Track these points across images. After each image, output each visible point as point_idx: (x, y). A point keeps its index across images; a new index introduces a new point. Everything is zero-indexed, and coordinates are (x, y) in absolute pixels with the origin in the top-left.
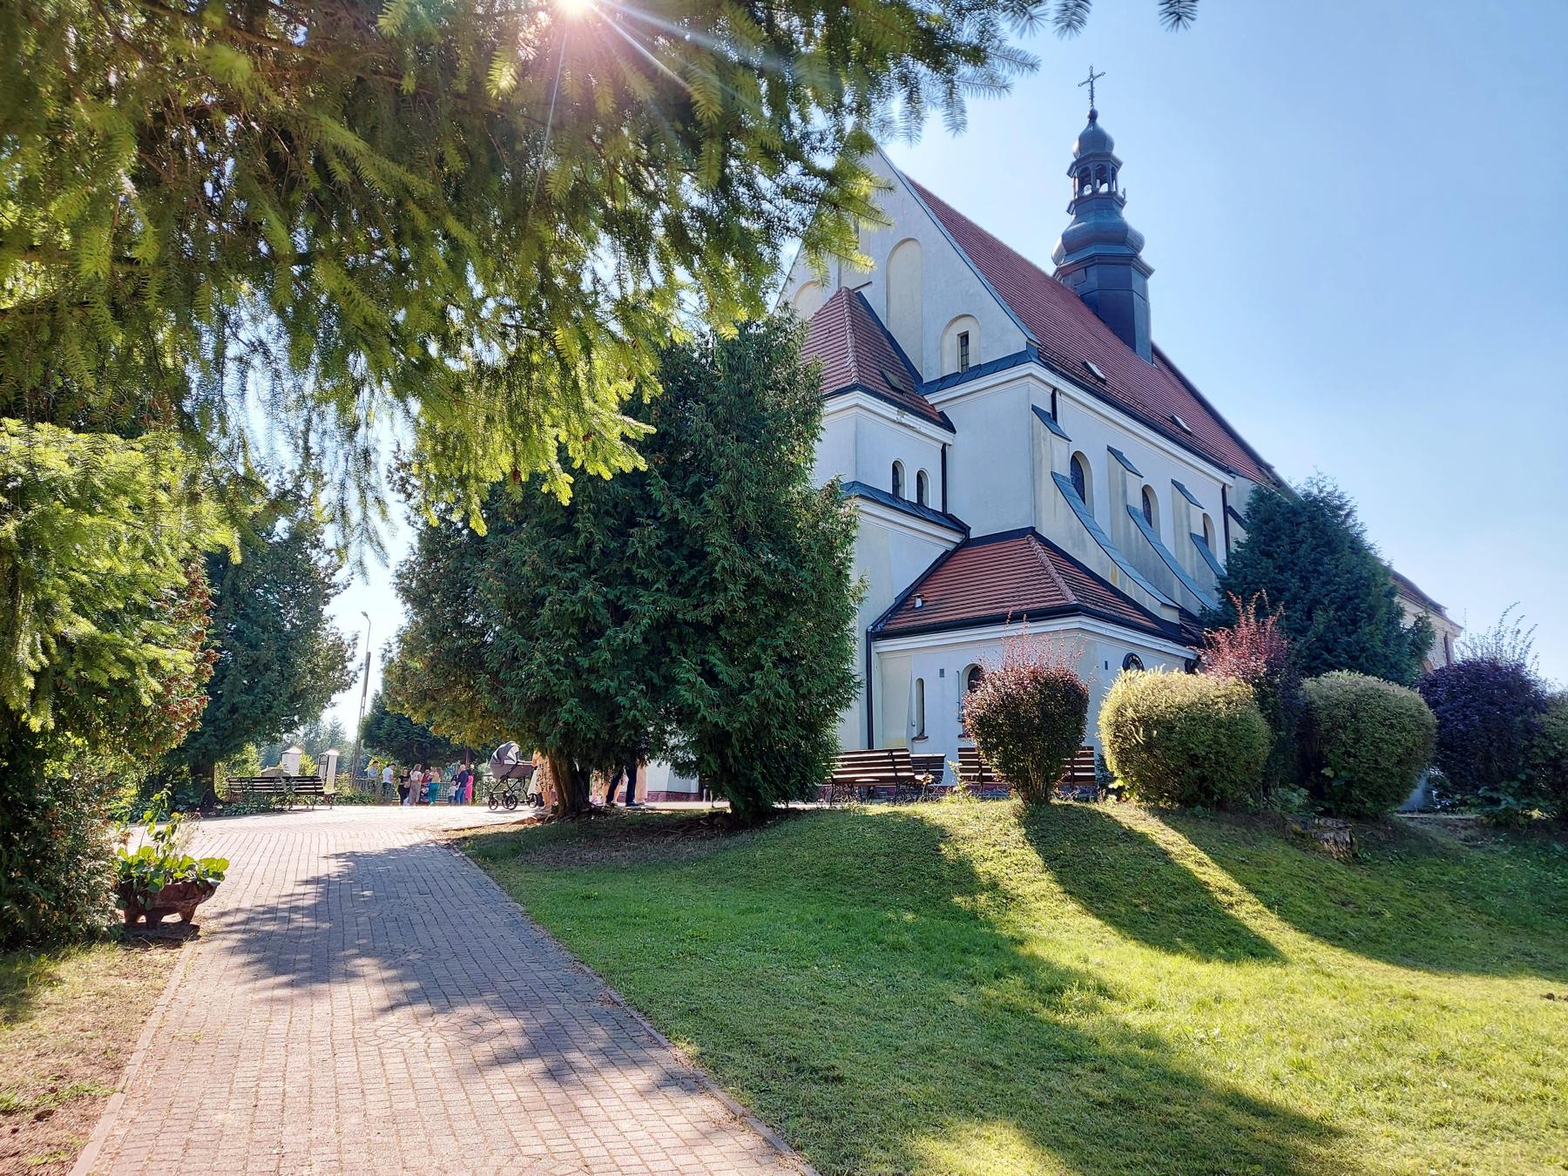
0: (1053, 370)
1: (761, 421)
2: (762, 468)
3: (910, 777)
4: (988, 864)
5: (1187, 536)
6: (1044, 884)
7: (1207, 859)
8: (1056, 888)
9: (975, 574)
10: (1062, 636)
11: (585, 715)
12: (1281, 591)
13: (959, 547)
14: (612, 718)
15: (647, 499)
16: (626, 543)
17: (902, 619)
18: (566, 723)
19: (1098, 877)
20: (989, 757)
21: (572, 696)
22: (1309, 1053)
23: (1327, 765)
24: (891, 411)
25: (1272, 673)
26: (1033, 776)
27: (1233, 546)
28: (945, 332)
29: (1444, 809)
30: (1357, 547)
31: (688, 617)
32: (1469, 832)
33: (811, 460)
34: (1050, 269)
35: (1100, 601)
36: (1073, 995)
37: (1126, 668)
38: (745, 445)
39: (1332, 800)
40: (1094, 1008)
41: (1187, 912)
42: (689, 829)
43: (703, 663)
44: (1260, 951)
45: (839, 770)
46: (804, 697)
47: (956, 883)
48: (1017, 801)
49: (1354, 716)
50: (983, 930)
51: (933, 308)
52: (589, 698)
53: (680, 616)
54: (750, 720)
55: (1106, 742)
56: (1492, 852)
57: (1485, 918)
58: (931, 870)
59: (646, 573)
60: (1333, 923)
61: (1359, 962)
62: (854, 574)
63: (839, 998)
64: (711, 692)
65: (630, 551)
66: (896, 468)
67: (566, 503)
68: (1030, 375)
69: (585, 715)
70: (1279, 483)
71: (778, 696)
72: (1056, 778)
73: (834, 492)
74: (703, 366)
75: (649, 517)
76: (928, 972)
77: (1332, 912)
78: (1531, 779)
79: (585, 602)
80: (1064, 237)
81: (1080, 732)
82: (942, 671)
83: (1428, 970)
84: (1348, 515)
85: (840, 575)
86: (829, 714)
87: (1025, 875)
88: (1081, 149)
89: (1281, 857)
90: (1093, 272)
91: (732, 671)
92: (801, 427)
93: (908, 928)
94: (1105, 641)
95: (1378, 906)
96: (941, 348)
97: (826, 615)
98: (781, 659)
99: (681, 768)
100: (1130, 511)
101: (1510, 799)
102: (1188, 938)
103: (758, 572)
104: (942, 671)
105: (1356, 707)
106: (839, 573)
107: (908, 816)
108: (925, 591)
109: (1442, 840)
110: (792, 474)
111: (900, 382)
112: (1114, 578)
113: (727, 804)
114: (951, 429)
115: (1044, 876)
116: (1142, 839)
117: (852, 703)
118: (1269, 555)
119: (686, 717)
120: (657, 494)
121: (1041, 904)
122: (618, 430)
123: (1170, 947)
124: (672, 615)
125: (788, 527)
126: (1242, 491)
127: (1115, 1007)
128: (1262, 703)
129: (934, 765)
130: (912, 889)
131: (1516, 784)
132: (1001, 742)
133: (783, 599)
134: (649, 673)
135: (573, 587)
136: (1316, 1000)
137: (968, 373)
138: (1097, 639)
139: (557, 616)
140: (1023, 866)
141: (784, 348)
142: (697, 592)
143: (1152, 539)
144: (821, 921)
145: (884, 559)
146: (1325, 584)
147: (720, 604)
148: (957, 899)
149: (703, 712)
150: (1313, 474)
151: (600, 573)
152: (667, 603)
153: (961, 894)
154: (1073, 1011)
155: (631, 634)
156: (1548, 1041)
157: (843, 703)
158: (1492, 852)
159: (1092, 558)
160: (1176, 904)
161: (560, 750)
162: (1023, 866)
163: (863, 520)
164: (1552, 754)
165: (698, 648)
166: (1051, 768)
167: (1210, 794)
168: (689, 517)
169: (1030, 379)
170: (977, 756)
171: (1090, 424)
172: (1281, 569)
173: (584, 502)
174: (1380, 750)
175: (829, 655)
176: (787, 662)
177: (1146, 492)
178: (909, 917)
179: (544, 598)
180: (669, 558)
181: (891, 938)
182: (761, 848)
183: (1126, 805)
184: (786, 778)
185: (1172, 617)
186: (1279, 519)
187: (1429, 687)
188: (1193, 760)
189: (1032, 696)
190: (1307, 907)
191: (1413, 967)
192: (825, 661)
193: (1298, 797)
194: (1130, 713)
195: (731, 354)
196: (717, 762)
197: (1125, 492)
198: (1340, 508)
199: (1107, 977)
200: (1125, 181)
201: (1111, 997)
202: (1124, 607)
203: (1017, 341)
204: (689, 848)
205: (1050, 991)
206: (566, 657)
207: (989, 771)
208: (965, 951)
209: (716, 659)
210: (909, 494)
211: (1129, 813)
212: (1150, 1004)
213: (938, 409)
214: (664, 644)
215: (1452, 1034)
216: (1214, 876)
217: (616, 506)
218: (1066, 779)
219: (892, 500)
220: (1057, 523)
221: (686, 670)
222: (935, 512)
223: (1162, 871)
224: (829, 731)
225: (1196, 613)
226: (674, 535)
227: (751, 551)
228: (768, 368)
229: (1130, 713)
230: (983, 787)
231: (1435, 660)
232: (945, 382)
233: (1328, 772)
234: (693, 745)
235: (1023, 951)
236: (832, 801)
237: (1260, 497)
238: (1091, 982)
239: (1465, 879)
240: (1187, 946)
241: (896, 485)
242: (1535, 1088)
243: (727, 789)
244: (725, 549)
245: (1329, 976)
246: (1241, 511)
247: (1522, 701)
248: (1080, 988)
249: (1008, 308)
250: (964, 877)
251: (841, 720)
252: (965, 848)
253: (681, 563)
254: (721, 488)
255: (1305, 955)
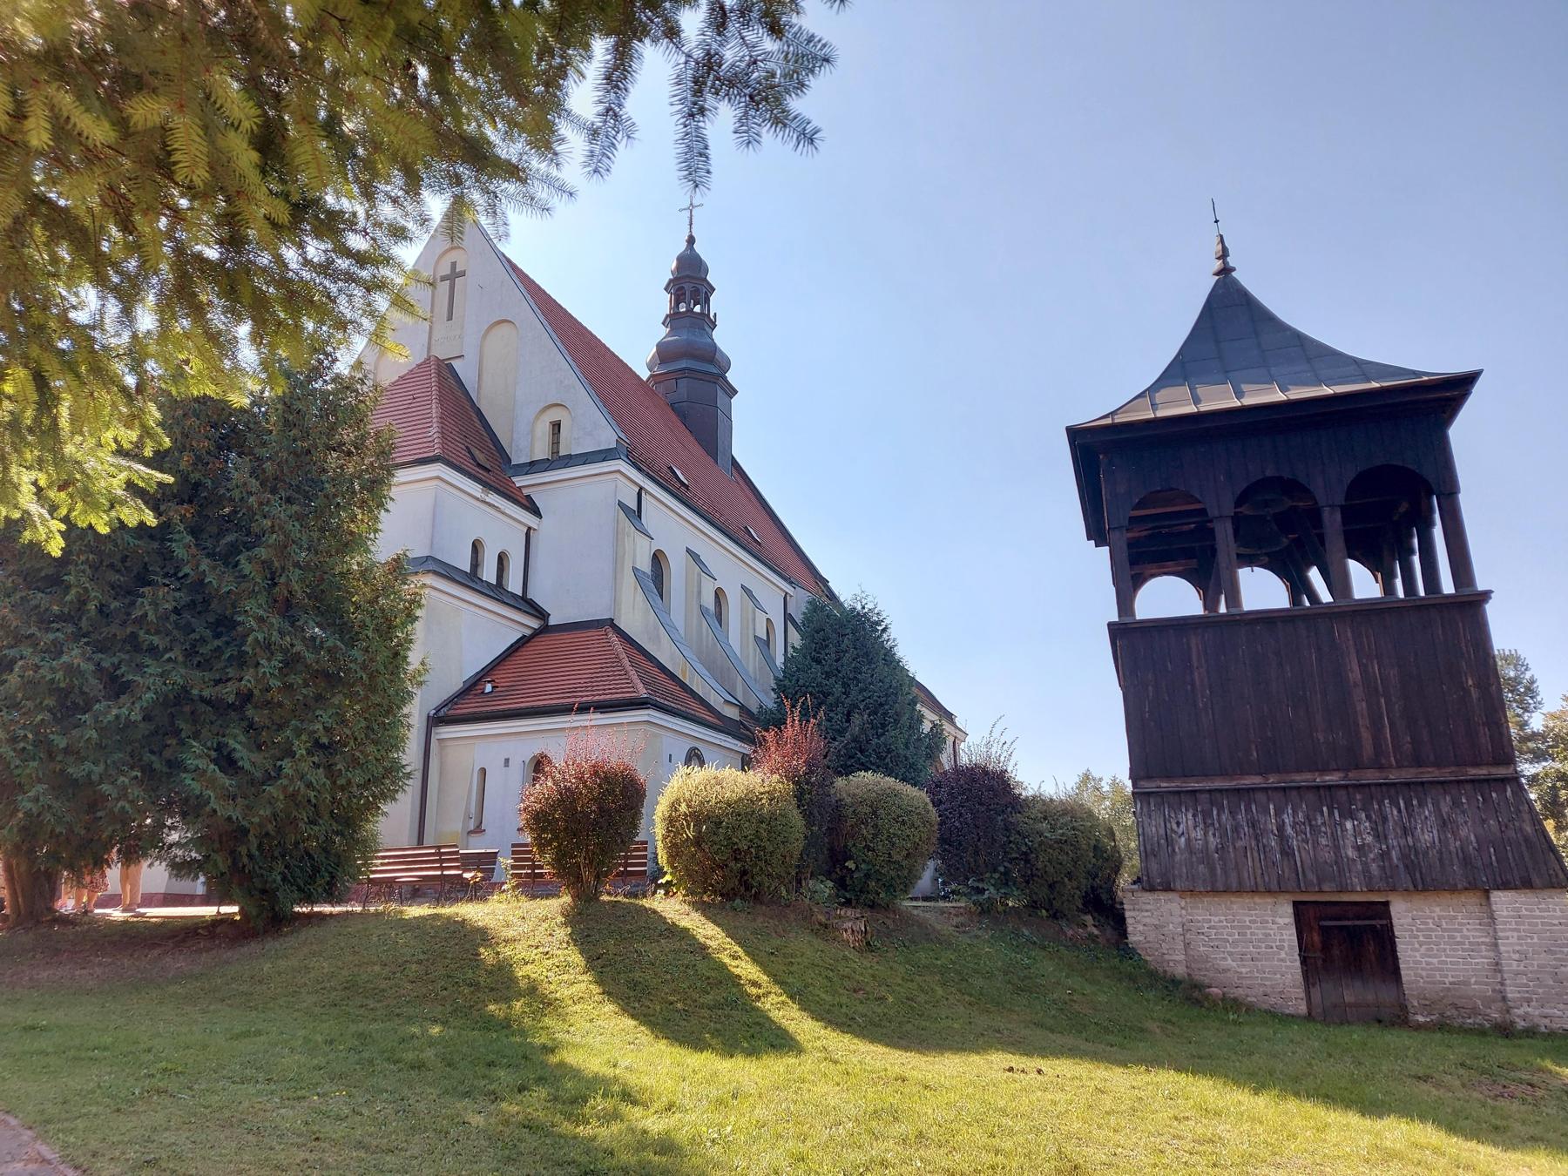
0: (640, 470)
1: (317, 483)
2: (316, 535)
3: (473, 876)
4: (529, 967)
5: (751, 638)
6: (583, 986)
7: (741, 952)
8: (595, 989)
9: (550, 663)
10: (626, 728)
11: (56, 804)
12: (826, 695)
13: (537, 633)
14: (93, 807)
15: (167, 556)
16: (133, 603)
17: (471, 703)
18: (28, 814)
19: (637, 975)
20: (542, 852)
21: (40, 781)
22: (809, 1143)
23: (851, 858)
24: (475, 489)
25: (810, 772)
26: (585, 873)
27: (790, 650)
28: (537, 418)
29: (945, 898)
30: (889, 659)
31: (206, 693)
32: (961, 919)
33: (376, 531)
34: (644, 374)
35: (668, 695)
36: (599, 1104)
37: (688, 762)
38: (295, 508)
39: (851, 892)
40: (615, 1116)
41: (718, 1006)
42: (184, 941)
43: (219, 748)
44: (782, 1042)
45: (381, 869)
46: (342, 788)
47: (492, 990)
48: (566, 899)
49: (874, 813)
50: (513, 1039)
51: (526, 393)
52: (65, 785)
53: (195, 692)
54: (275, 815)
55: (659, 837)
56: (977, 937)
57: (967, 998)
58: (468, 977)
59: (156, 640)
60: (844, 1010)
61: (863, 1046)
62: (414, 658)
63: (338, 1131)
64: (226, 781)
65: (137, 613)
66: (476, 547)
67: (57, 553)
68: (619, 471)
69: (56, 804)
70: (832, 596)
71: (309, 785)
72: (606, 875)
73: (399, 567)
74: (255, 416)
75: (166, 575)
76: (446, 1092)
77: (844, 1000)
78: (1006, 873)
79: (70, 670)
80: (658, 345)
81: (635, 827)
82: (507, 760)
83: (918, 1051)
84: (884, 630)
85: (397, 657)
86: (372, 807)
87: (566, 977)
88: (678, 268)
89: (804, 945)
90: (683, 383)
91: (257, 757)
92: (366, 495)
93: (432, 1042)
94: (670, 734)
95: (883, 991)
96: (532, 431)
97: (377, 699)
98: (318, 745)
99: (180, 868)
100: (703, 611)
101: (992, 889)
102: (716, 1033)
103: (299, 647)
104: (507, 760)
105: (876, 806)
106: (397, 654)
107: (449, 918)
108: (499, 675)
109: (938, 927)
110: (353, 543)
111: (484, 457)
112: (684, 672)
113: (235, 909)
114: (536, 512)
115: (585, 977)
116: (685, 933)
117: (399, 796)
118: (818, 662)
119: (191, 809)
120: (180, 552)
121: (577, 1008)
122: (123, 476)
123: (698, 1045)
124: (185, 690)
125: (340, 600)
126: (800, 601)
127: (637, 1112)
128: (799, 800)
129: (485, 862)
130: (444, 998)
131: (996, 876)
132: (556, 838)
133: (331, 679)
134: (148, 757)
135: (56, 650)
136: (822, 1088)
137: (558, 461)
138: (662, 732)
139: (28, 684)
140: (565, 967)
141: (354, 410)
142: (222, 665)
143: (722, 640)
144: (331, 1042)
145: (452, 639)
146: (861, 691)
147: (249, 679)
148: (492, 1007)
149: (213, 804)
150: (858, 592)
151: (95, 636)
152: (178, 676)
153: (496, 1001)
154: (593, 1122)
155: (129, 710)
156: (1004, 1113)
157: (389, 796)
158: (977, 937)
159: (664, 653)
160: (708, 999)
161: (17, 847)
162: (565, 967)
163: (428, 596)
164: (1024, 849)
165: (215, 729)
166: (602, 863)
167: (748, 888)
168: (218, 580)
169: (618, 476)
170: (530, 852)
171: (672, 527)
172: (828, 675)
173: (81, 552)
174: (893, 844)
175: (375, 743)
176: (324, 748)
177: (719, 595)
178: (435, 1030)
179: (13, 662)
180: (189, 624)
181: (410, 1056)
182: (274, 960)
183: (673, 900)
184: (312, 878)
185: (732, 713)
186: (828, 629)
187: (934, 788)
188: (737, 854)
189: (591, 790)
190: (823, 996)
191: (906, 1049)
192: (370, 749)
193: (826, 888)
194: (683, 808)
195: (288, 407)
196: (229, 860)
197: (699, 593)
198: (878, 623)
199: (633, 1080)
200: (717, 305)
201: (635, 1103)
202: (694, 705)
203: (607, 437)
204: (178, 962)
205: (573, 1101)
206: (36, 734)
207: (541, 867)
208: (490, 1064)
209: (237, 744)
210: (489, 573)
211: (673, 908)
212: (670, 1107)
213: (526, 492)
214: (172, 724)
215: (930, 1111)
216: (746, 969)
217: (124, 559)
218: (618, 875)
219: (470, 579)
220: (635, 617)
221: (197, 756)
222: (514, 595)
223: (699, 967)
224: (369, 826)
225: (755, 711)
226: (199, 598)
227: (292, 624)
228: (333, 428)
229: (683, 808)
230: (533, 886)
231: (945, 760)
232: (533, 467)
233: (850, 864)
234: (197, 843)
235: (554, 1059)
236: (365, 903)
237: (814, 608)
238: (616, 1088)
239: (953, 963)
240: (714, 1042)
241: (476, 563)
242: (988, 1158)
243: (236, 890)
244: (261, 620)
245: (836, 1062)
246: (799, 618)
247: (1003, 802)
248: (604, 1096)
249: (601, 405)
250: (502, 981)
251: (385, 814)
252: (507, 951)
253: (201, 630)
254: (263, 552)
255: (818, 1044)
